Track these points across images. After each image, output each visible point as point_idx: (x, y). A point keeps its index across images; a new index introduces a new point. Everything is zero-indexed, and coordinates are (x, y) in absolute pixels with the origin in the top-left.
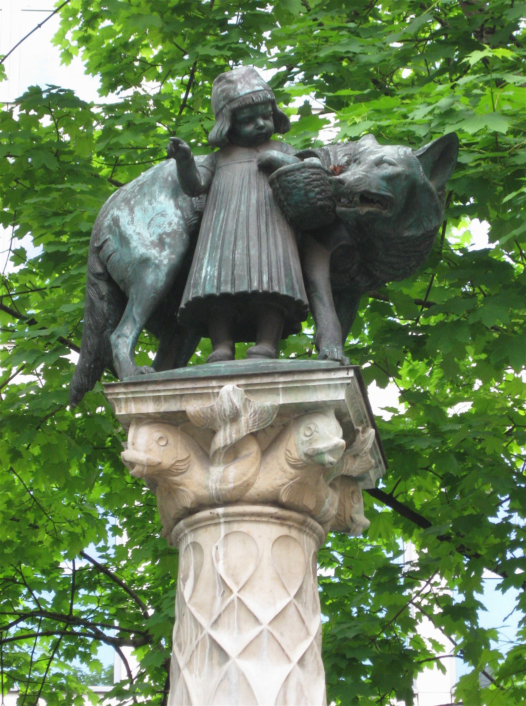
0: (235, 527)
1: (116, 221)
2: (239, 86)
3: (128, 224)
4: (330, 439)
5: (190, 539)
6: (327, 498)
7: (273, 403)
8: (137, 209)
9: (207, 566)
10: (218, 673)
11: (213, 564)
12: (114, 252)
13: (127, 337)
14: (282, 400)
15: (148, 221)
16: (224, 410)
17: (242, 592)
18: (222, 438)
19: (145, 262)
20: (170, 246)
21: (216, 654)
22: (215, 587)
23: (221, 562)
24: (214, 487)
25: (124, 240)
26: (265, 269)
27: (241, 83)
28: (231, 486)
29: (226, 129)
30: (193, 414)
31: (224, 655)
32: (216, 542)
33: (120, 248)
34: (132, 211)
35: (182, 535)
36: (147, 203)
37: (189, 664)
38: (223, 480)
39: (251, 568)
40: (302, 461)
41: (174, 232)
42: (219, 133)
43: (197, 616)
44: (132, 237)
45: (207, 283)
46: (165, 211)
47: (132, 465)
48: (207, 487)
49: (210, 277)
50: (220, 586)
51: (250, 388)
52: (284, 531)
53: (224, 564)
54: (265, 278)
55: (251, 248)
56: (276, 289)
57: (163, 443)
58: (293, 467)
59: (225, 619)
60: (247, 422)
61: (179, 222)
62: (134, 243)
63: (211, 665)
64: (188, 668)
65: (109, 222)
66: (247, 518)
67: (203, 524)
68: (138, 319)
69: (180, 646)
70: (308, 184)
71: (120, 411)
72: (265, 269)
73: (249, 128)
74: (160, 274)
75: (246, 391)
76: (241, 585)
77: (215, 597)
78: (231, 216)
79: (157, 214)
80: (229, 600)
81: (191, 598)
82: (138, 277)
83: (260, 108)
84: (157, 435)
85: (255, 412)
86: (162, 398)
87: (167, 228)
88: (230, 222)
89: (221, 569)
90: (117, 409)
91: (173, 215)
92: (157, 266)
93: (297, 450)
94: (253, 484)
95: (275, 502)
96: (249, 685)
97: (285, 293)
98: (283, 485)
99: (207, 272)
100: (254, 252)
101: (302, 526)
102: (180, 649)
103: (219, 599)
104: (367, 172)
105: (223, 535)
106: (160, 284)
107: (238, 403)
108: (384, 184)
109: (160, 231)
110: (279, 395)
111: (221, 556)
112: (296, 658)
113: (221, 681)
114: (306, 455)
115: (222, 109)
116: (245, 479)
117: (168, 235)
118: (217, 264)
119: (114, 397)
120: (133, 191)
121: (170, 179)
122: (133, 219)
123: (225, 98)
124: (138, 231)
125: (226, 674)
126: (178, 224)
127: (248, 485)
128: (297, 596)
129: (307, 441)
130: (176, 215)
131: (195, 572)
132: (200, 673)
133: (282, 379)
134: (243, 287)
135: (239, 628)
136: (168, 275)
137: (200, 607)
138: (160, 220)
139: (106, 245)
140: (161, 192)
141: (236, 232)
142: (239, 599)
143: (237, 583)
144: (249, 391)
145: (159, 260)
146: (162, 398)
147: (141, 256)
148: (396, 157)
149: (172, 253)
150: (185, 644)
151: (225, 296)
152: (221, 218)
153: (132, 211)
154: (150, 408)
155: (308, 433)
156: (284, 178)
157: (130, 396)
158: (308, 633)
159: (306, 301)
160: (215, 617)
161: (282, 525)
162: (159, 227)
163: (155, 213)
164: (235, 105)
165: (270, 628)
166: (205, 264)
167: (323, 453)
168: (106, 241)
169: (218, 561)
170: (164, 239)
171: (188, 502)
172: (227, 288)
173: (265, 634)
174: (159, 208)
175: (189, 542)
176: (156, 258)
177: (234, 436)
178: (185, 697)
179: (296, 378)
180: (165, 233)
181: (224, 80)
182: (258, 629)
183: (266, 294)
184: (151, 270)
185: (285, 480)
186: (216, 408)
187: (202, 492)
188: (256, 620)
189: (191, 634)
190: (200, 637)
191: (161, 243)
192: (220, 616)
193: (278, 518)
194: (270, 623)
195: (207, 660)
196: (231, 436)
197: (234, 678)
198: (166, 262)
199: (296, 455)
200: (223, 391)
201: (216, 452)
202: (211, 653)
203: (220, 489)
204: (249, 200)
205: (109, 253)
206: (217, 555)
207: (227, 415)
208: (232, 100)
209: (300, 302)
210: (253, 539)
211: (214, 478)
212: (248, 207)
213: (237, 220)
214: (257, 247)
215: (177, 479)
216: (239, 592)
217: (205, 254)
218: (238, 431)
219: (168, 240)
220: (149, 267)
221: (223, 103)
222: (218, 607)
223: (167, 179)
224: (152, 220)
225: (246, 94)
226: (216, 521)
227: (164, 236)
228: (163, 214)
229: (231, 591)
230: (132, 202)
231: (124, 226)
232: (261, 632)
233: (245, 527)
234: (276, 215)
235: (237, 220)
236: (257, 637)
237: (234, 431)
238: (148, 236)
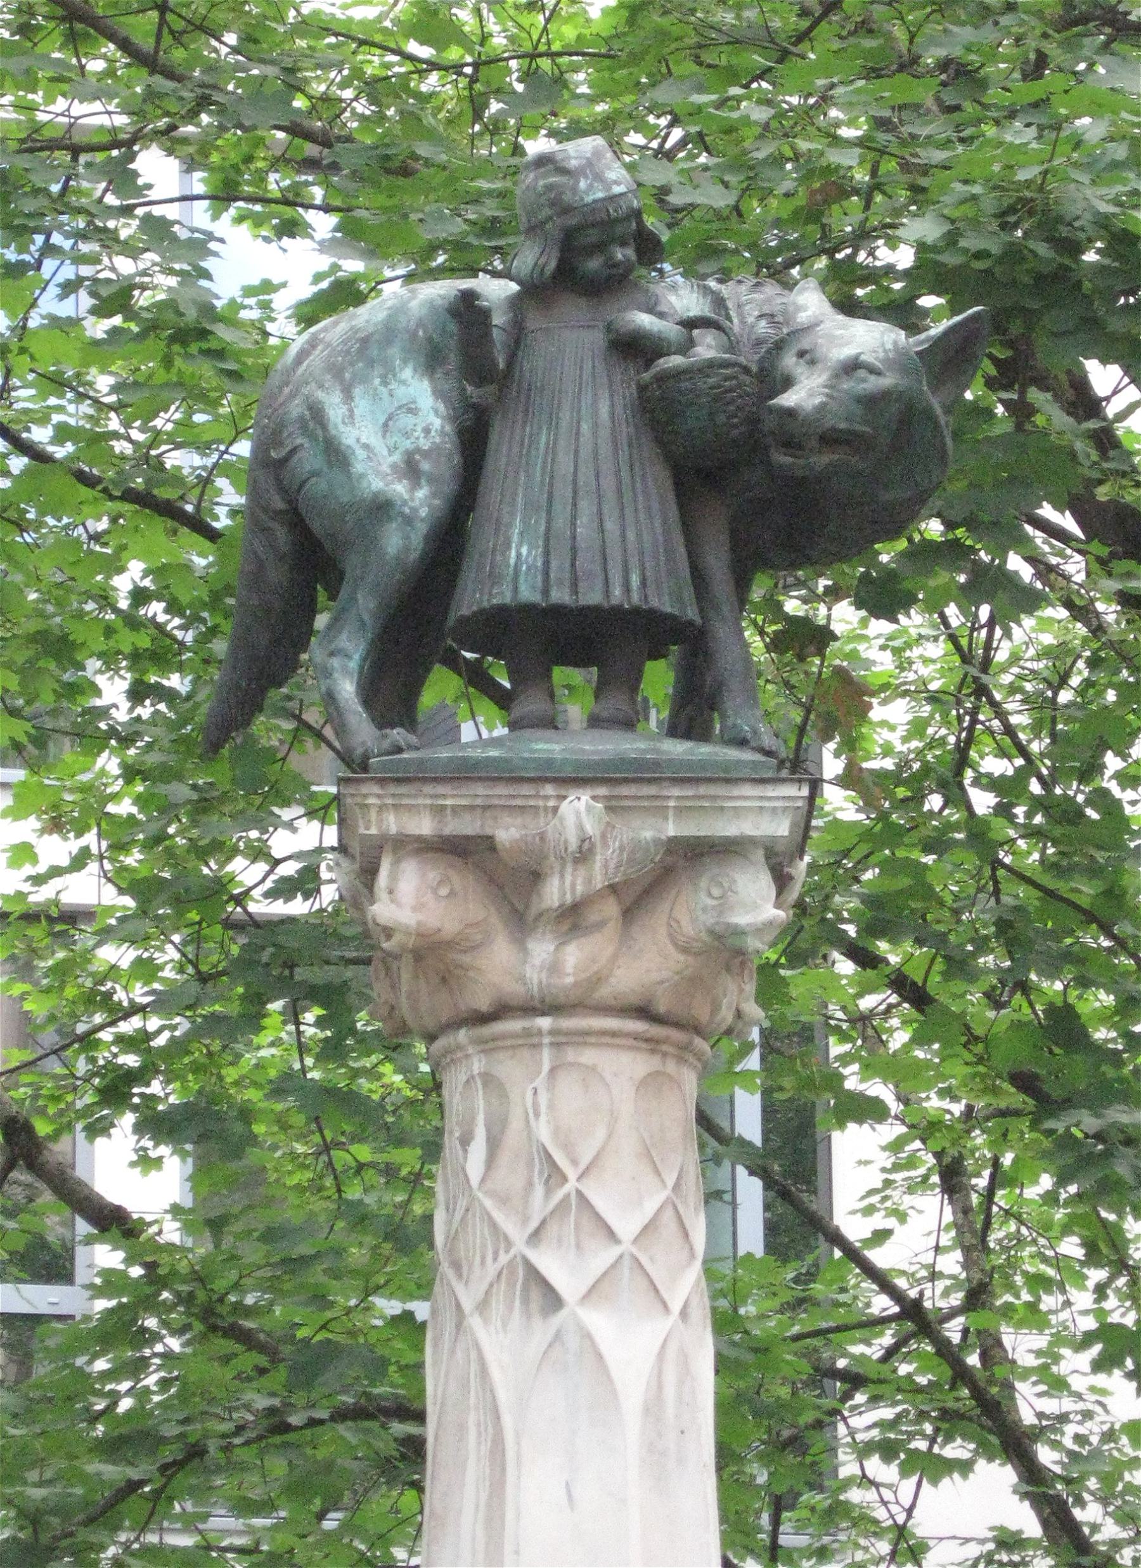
0: (571, 1055)
2: (583, 184)
3: (344, 423)
4: (755, 907)
5: (477, 1065)
6: (725, 995)
7: (658, 835)
8: (357, 391)
9: (516, 1123)
10: (542, 1331)
11: (527, 1121)
12: (315, 474)
13: (348, 656)
14: (671, 829)
15: (382, 420)
16: (566, 842)
17: (585, 1180)
18: (555, 890)
19: (382, 508)
20: (431, 480)
21: (535, 1294)
22: (530, 1165)
23: (543, 1118)
24: (535, 981)
26: (634, 562)
27: (586, 177)
28: (569, 980)
29: (553, 264)
30: (507, 845)
31: (552, 1300)
32: (532, 1080)
33: (325, 469)
34: (348, 397)
35: (459, 1055)
36: (377, 381)
37: (483, 1306)
38: (554, 968)
39: (601, 1133)
40: (703, 942)
41: (435, 450)
42: (537, 270)
43: (499, 1217)
44: (353, 453)
45: (522, 579)
46: (414, 402)
47: (388, 932)
48: (522, 979)
49: (529, 568)
50: (541, 1163)
51: (614, 803)
53: (548, 1122)
54: (635, 580)
55: (606, 518)
56: (654, 602)
57: (444, 891)
58: (684, 950)
59: (552, 1229)
60: (606, 866)
61: (443, 427)
62: (358, 467)
63: (527, 1314)
64: (481, 1314)
65: (299, 410)
66: (593, 1040)
67: (508, 1043)
68: (366, 617)
69: (457, 1266)
70: (716, 399)
71: (367, 828)
72: (634, 562)
73: (594, 264)
74: (413, 536)
75: (609, 809)
76: (583, 1166)
77: (530, 1184)
78: (562, 443)
79: (400, 407)
80: (560, 1194)
81: (483, 1180)
82: (372, 543)
83: (619, 230)
84: (433, 875)
85: (622, 849)
86: (449, 811)
87: (422, 441)
88: (561, 455)
89: (543, 1132)
90: (361, 823)
91: (432, 414)
92: (408, 521)
93: (694, 920)
94: (608, 977)
95: (643, 1012)
96: (599, 1357)
97: (669, 610)
98: (662, 982)
99: (519, 555)
100: (611, 525)
101: (683, 1052)
102: (460, 1276)
103: (539, 1190)
104: (831, 387)
105: (546, 1067)
106: (414, 556)
107: (591, 828)
108: (858, 410)
109: (408, 444)
110: (666, 818)
111: (543, 1109)
112: (676, 1306)
113: (550, 1346)
114: (711, 932)
115: (543, 223)
116: (595, 968)
117: (426, 454)
118: (541, 543)
119: (359, 800)
120: (348, 352)
121: (421, 333)
122: (351, 411)
123: (552, 204)
124: (364, 440)
125: (558, 1336)
126: (442, 433)
127: (598, 980)
128: (677, 1187)
129: (714, 907)
130: (436, 412)
131: (488, 1131)
132: (505, 1325)
133: (676, 791)
134: (592, 596)
135: (578, 1246)
136: (427, 538)
137: (503, 1200)
138: (407, 421)
139: (295, 459)
140: (405, 362)
141: (575, 482)
142: (579, 1193)
143: (574, 1162)
145: (411, 508)
146: (449, 811)
147: (376, 495)
148: (881, 355)
149: (434, 495)
150: (470, 1267)
151: (557, 612)
152: (542, 446)
153: (348, 397)
154: (424, 826)
155: (716, 892)
156: (671, 383)
157: (389, 801)
158: (692, 1255)
159: (698, 621)
160: (534, 1224)
161: (653, 1051)
162: (407, 435)
163: (396, 404)
164: (572, 221)
165: (634, 1250)
166: (515, 538)
167: (744, 933)
168: (294, 451)
169: (537, 1114)
170: (417, 463)
171: (483, 1003)
172: (560, 595)
173: (627, 1262)
174: (401, 392)
175: (476, 1072)
176: (405, 503)
177: (579, 888)
178: (474, 1367)
179: (703, 790)
180: (418, 450)
181: (550, 167)
182: (616, 1251)
183: (636, 611)
184: (394, 525)
185: (665, 974)
186: (550, 835)
187: (512, 989)
188: (611, 1235)
189: (484, 1246)
190: (504, 1259)
191: (410, 469)
192: (543, 1223)
193: (647, 1040)
194: (636, 1240)
195: (517, 1303)
196: (573, 886)
197: (572, 1341)
198: (423, 512)
199: (688, 929)
200: (565, 806)
201: (541, 915)
202: (526, 1289)
203: (549, 985)
204: (596, 413)
205: (304, 477)
206: (536, 1106)
207: (570, 850)
208: (567, 210)
209: (691, 623)
210: (602, 1079)
211: (537, 961)
212: (596, 425)
213: (576, 452)
214: (616, 513)
215: (466, 959)
216: (579, 1179)
217: (512, 514)
218: (589, 881)
219: (425, 466)
220: (390, 519)
221: (546, 212)
222: (539, 1205)
223: (416, 331)
224: (390, 418)
225: (595, 201)
226: (535, 1040)
227: (417, 457)
228: (411, 409)
229: (565, 1179)
230: (347, 376)
231: (336, 428)
232: (621, 1257)
233: (588, 1056)
234: (649, 449)
235: (576, 452)
236: (614, 1266)
237: (579, 881)
238: (385, 452)
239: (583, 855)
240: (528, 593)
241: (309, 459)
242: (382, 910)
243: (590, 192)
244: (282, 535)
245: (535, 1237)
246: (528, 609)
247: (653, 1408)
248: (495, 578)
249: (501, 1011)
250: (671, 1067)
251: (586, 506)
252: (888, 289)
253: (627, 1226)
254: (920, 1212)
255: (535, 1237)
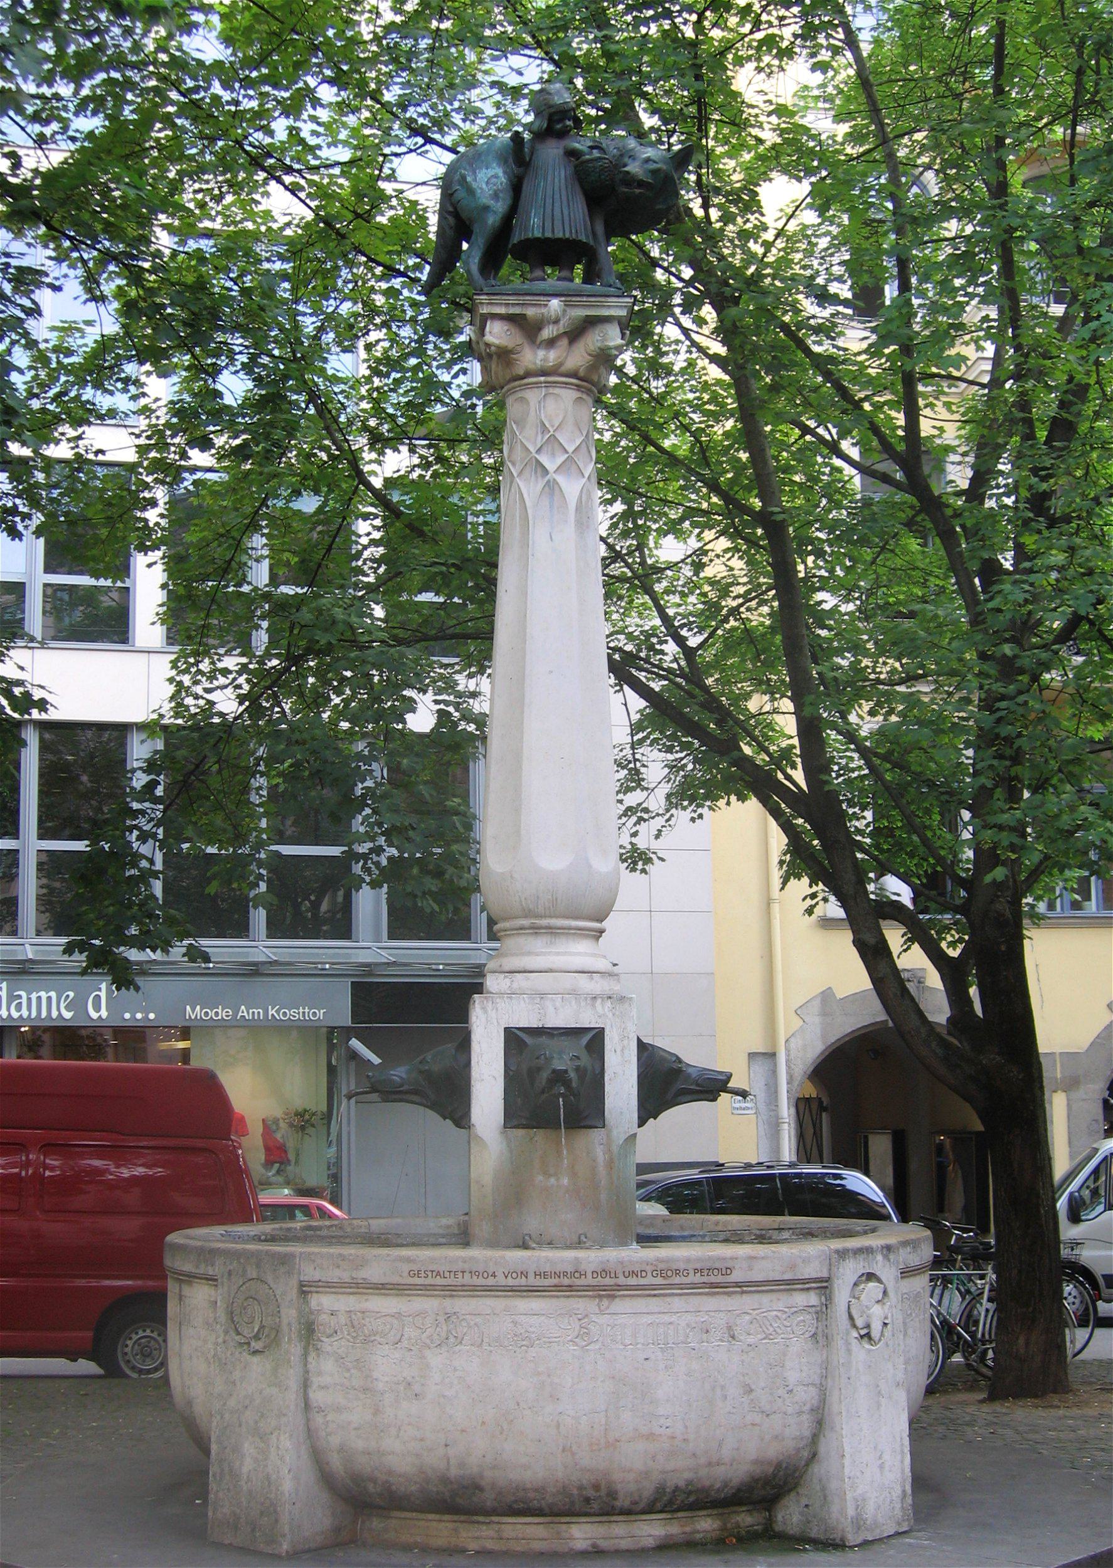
0: (551, 390)
1: (464, 178)
19: (486, 208)
21: (539, 470)
25: (471, 191)
31: (545, 471)
37: (520, 474)
38: (545, 360)
52: (579, 395)
73: (559, 126)
100: (566, 212)
127: (561, 364)
137: (528, 439)
138: (494, 180)
144: (567, 305)
154: (502, 310)
171: (521, 372)
187: (531, 366)
191: (496, 196)
208: (551, 107)
233: (557, 391)
234: (578, 188)
239: (556, 321)
240: (538, 234)
241: (461, 194)
242: (489, 338)
243: (558, 100)
244: (451, 220)
245: (539, 451)
246: (538, 239)
247: (578, 508)
248: (526, 229)
249: (528, 374)
250: (584, 396)
251: (557, 205)
252: (108, 21)
253: (570, 449)
254: (662, 860)
255: (539, 451)
